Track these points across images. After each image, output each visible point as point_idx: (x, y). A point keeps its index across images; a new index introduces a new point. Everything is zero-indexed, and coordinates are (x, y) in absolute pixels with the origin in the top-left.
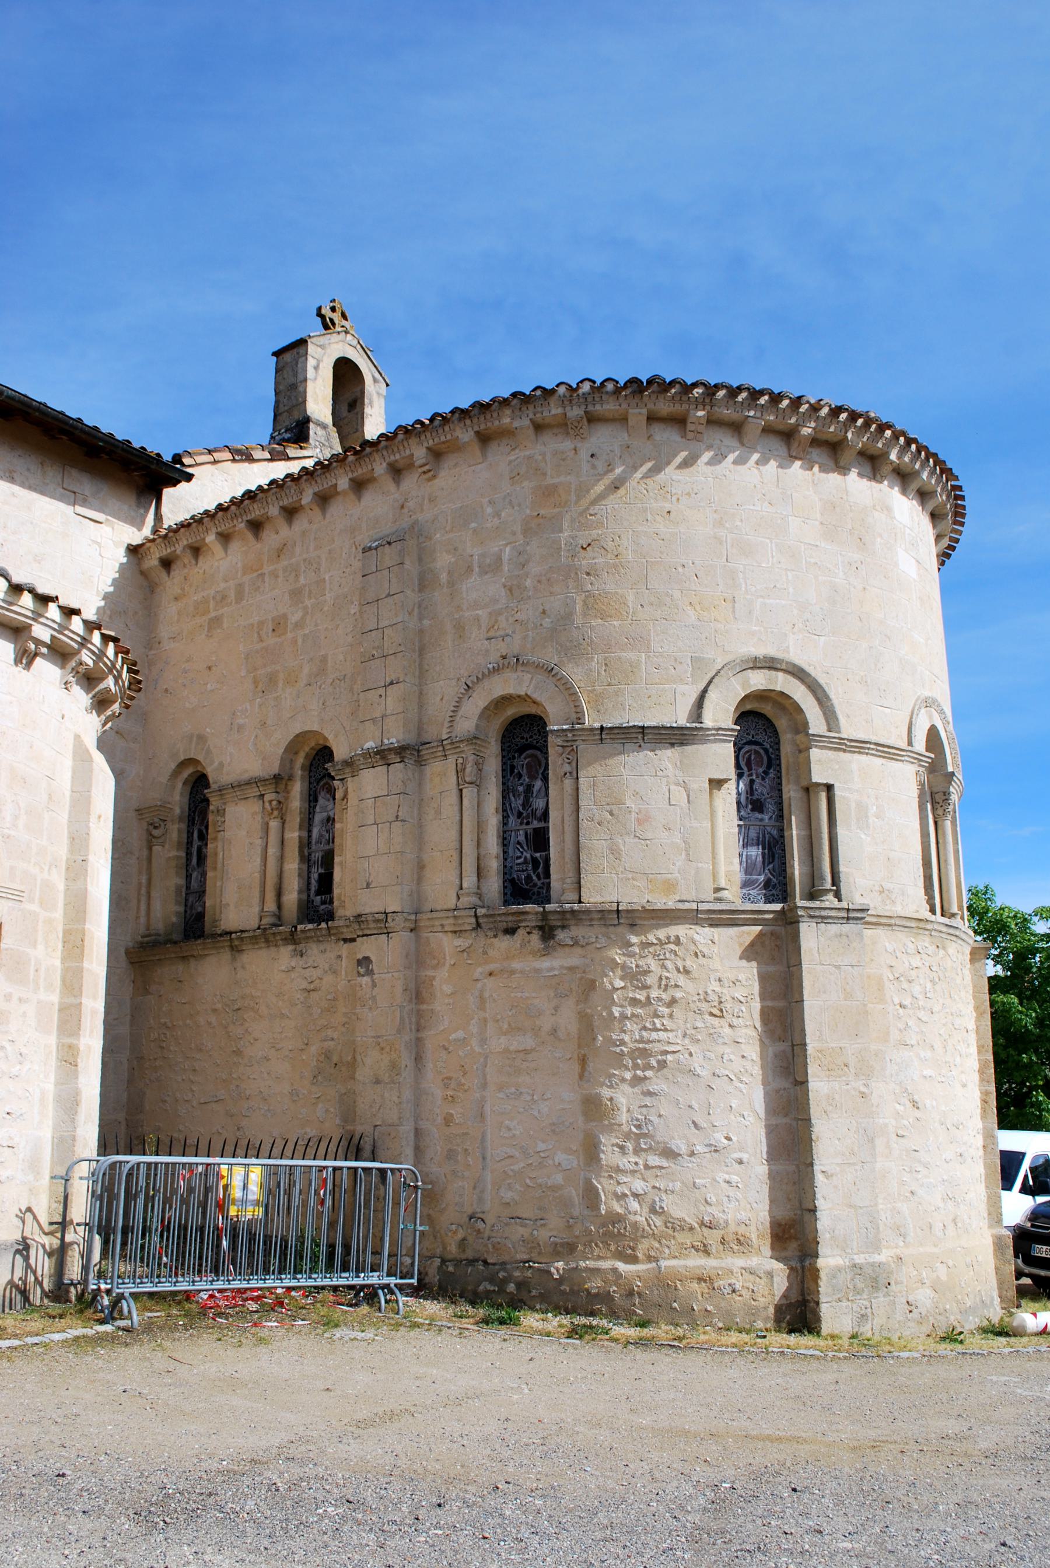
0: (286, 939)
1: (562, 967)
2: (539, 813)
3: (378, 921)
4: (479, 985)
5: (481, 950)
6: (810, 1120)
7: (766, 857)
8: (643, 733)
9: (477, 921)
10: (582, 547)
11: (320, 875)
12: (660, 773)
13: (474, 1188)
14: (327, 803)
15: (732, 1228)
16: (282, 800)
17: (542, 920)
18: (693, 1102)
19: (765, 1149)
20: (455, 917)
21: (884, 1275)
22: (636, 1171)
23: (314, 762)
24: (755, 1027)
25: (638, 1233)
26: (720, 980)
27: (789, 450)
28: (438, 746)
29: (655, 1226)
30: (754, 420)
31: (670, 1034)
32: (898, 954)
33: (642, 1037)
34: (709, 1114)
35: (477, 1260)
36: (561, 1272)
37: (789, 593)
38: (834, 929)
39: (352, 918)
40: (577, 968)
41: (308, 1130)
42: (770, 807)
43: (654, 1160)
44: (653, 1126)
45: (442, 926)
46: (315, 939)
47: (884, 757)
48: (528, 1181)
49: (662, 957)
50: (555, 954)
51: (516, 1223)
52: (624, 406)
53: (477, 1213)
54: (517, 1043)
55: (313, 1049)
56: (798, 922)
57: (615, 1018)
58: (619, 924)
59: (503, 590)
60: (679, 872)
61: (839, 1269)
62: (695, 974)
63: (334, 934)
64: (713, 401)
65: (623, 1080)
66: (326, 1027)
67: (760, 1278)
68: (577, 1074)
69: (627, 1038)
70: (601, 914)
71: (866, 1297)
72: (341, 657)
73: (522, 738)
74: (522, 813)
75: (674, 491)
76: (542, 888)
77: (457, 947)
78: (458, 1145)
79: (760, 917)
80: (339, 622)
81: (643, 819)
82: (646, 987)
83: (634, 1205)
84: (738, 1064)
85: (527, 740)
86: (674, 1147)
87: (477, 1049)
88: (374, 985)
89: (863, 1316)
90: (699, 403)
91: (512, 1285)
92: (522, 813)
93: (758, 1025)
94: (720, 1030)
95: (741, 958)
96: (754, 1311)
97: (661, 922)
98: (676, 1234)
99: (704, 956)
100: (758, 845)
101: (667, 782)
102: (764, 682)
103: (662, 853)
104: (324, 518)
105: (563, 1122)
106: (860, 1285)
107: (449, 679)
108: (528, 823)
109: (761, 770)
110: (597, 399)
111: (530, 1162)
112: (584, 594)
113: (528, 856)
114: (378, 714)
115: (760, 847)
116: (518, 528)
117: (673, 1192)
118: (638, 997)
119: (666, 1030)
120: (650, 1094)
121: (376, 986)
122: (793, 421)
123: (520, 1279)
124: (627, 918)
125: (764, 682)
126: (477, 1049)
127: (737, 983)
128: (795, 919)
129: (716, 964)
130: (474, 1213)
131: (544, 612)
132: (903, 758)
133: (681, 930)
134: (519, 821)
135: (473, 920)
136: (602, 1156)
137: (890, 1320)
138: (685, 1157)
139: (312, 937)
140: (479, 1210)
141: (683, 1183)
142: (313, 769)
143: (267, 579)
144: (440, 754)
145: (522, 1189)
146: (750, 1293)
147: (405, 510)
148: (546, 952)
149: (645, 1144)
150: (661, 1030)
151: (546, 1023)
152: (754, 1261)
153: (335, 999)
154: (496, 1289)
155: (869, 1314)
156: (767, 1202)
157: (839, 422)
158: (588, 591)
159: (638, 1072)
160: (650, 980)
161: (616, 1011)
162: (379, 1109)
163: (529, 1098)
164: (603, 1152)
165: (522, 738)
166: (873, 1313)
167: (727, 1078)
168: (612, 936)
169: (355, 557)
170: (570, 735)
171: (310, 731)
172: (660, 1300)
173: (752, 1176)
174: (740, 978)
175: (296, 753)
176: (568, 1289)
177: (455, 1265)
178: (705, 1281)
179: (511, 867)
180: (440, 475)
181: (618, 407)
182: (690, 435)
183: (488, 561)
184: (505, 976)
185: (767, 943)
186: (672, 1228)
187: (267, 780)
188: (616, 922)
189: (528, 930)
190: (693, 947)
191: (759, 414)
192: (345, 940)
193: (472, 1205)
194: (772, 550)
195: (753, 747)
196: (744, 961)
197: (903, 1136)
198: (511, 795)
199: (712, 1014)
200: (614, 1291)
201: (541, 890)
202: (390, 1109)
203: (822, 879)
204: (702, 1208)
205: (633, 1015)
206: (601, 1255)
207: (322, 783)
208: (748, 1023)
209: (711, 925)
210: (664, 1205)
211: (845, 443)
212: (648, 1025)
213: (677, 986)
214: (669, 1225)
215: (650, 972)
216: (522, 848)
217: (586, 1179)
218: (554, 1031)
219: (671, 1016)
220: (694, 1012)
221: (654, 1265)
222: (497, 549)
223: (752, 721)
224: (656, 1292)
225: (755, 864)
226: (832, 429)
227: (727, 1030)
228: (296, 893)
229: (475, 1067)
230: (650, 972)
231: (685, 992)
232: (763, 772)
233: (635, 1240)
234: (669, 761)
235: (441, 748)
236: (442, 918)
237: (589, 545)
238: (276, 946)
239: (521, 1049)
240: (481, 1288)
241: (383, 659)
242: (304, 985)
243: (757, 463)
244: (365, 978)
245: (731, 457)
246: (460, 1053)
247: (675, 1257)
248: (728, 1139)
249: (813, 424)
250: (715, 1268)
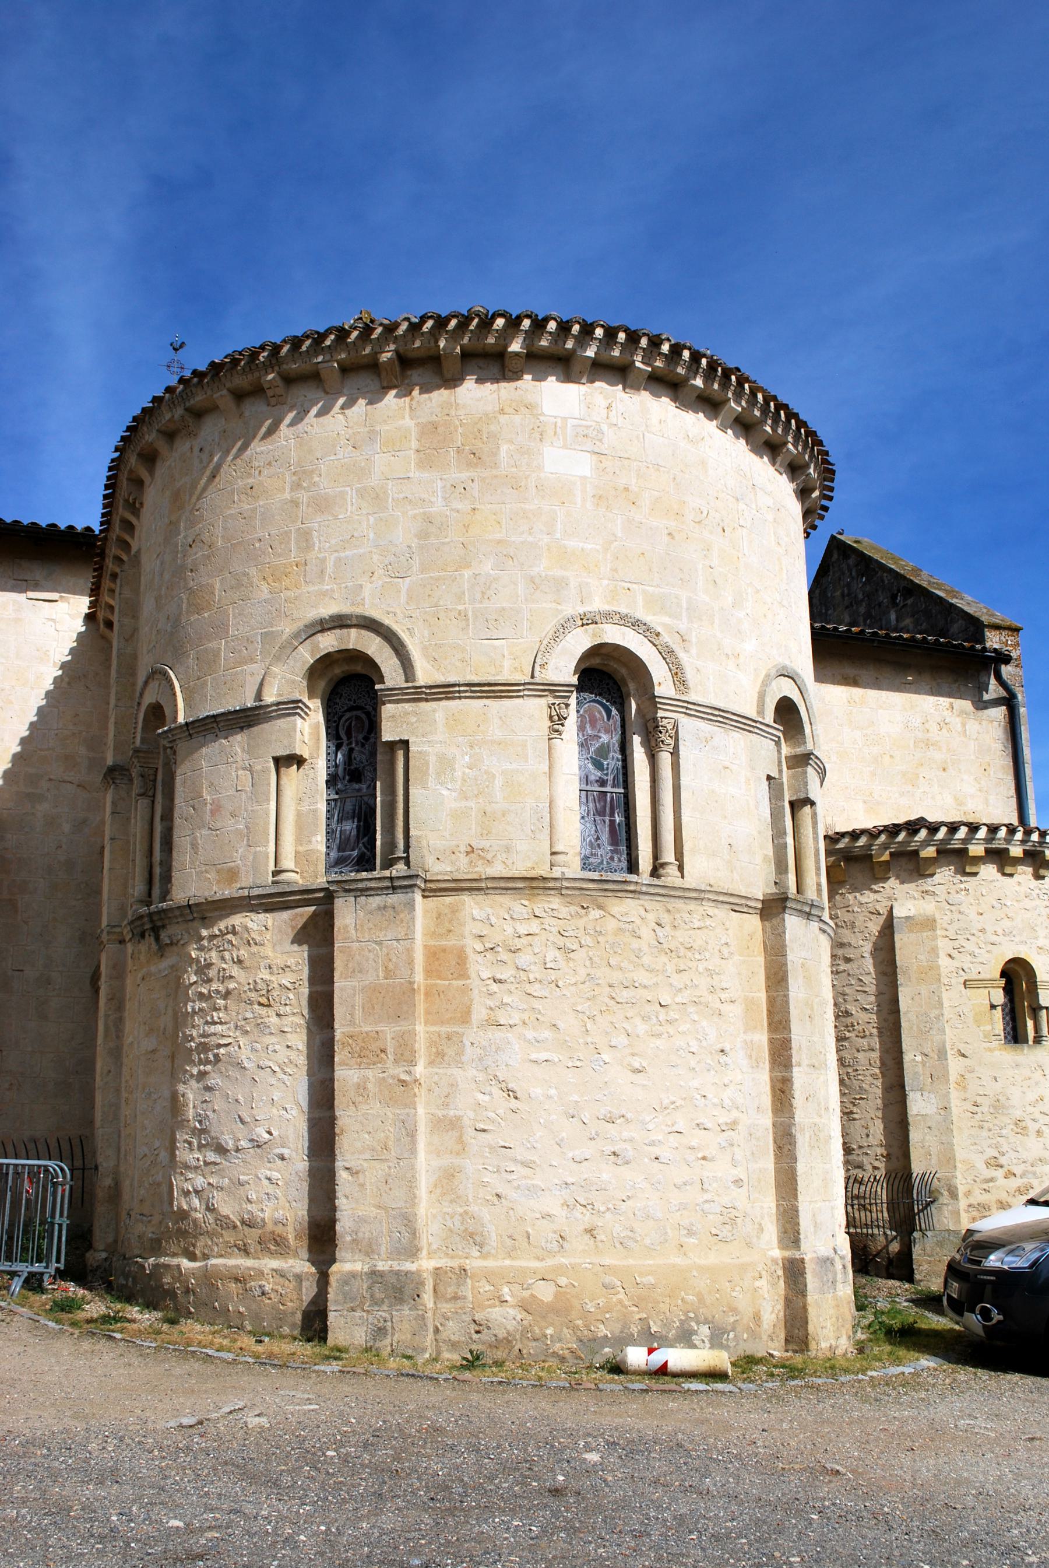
7: (362, 829)
8: (215, 721)
15: (270, 1227)
18: (240, 1097)
19: (306, 1145)
21: (411, 1286)
24: (303, 1015)
25: (198, 1231)
26: (270, 968)
30: (325, 365)
31: (225, 1027)
32: (493, 920)
37: (369, 539)
38: (376, 901)
43: (212, 1157)
44: (209, 1121)
47: (487, 697)
49: (221, 949)
52: (209, 393)
58: (194, 919)
60: (241, 860)
61: (353, 1275)
62: (247, 964)
65: (192, 1076)
71: (386, 1308)
83: (196, 1202)
84: (283, 1054)
86: (223, 1143)
89: (380, 1329)
90: (269, 366)
93: (305, 1012)
94: (266, 1020)
95: (292, 943)
97: (224, 913)
98: (223, 1232)
99: (256, 944)
100: (353, 818)
102: (335, 643)
103: (227, 842)
106: (379, 1295)
109: (360, 737)
110: (189, 394)
115: (356, 820)
117: (222, 1188)
119: (221, 1023)
120: (208, 1089)
122: (368, 350)
124: (197, 912)
125: (335, 643)
129: (268, 951)
132: (521, 694)
133: (237, 920)
137: (417, 1337)
138: (233, 1153)
146: (279, 1297)
155: (389, 1329)
156: (306, 1201)
157: (423, 334)
166: (393, 1328)
174: (289, 964)
178: (240, 1281)
181: (205, 396)
182: (273, 401)
190: (246, 936)
191: (328, 357)
194: (352, 498)
195: (355, 713)
196: (296, 945)
197: (484, 1131)
199: (260, 1004)
204: (244, 1206)
208: (295, 1011)
209: (266, 911)
210: (215, 1202)
213: (231, 977)
214: (218, 1222)
223: (355, 685)
225: (349, 839)
226: (417, 344)
227: (274, 1019)
231: (237, 982)
232: (363, 739)
233: (195, 1237)
234: (239, 746)
243: (342, 408)
245: (314, 411)
247: (221, 1256)
249: (392, 347)
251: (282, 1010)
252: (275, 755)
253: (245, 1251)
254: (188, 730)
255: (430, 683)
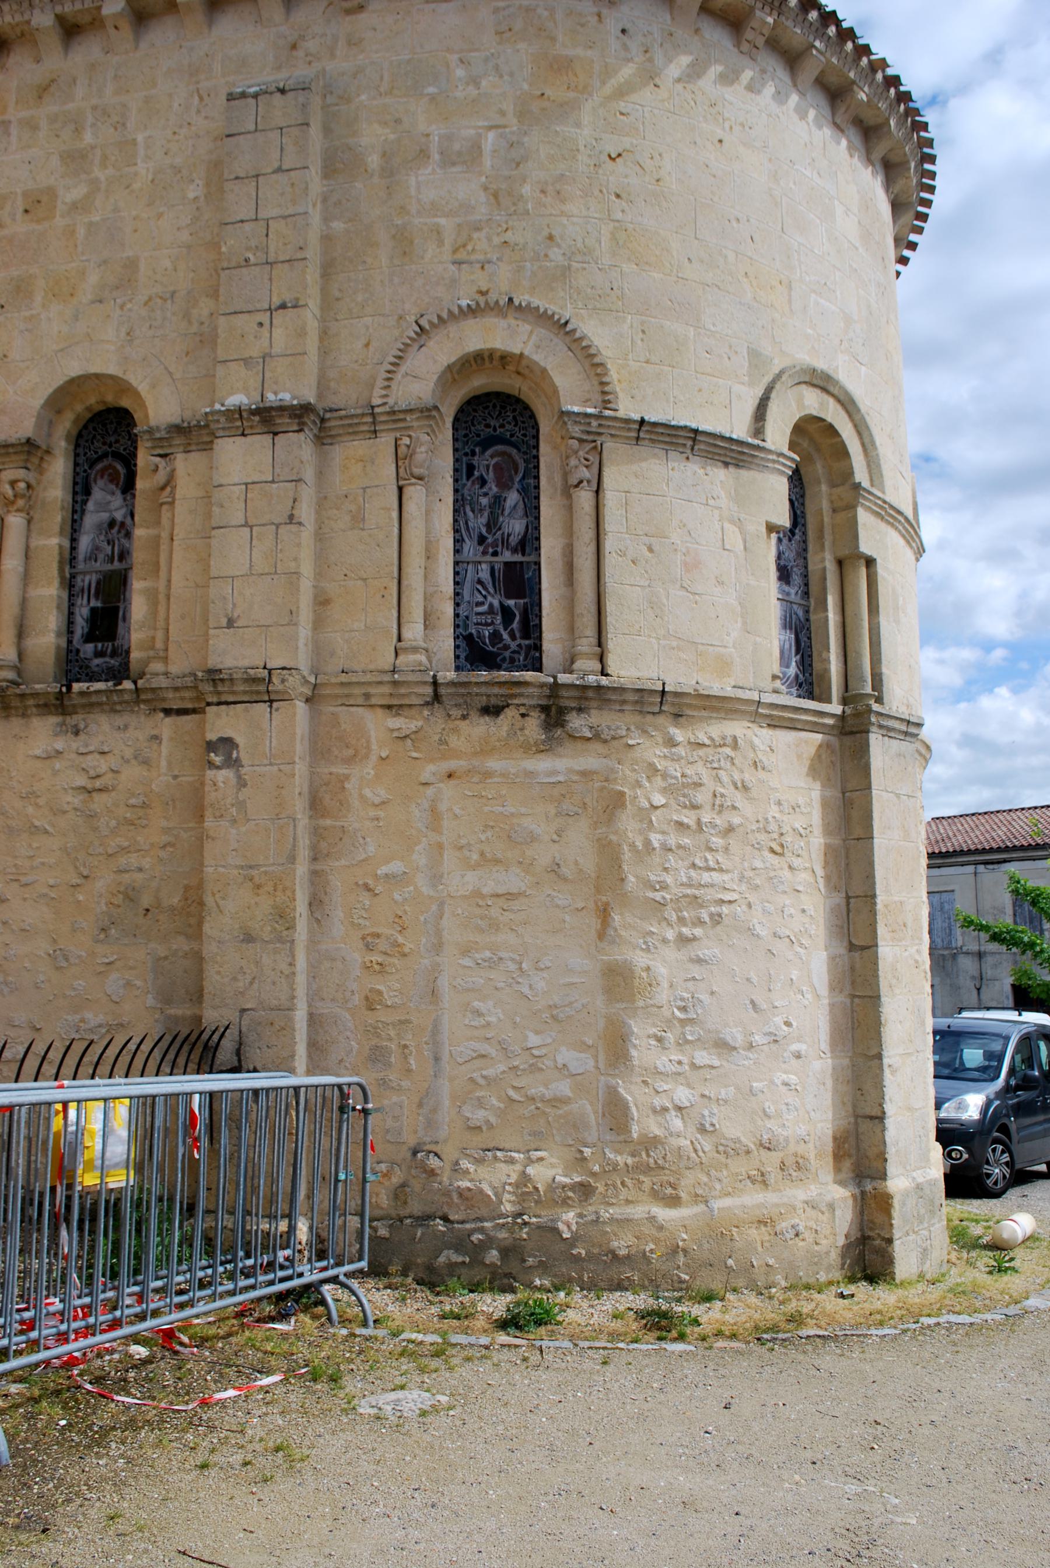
0: (46, 705)
1: (570, 771)
2: (514, 540)
3: (255, 680)
4: (430, 791)
5: (436, 738)
6: (879, 997)
8: (694, 440)
9: (436, 692)
10: (610, 156)
11: (93, 610)
12: (711, 502)
13: (420, 1105)
14: (109, 497)
15: (792, 1148)
16: (33, 482)
17: (549, 697)
20: (395, 683)
22: (679, 1074)
23: (84, 433)
27: (833, 114)
28: (363, 415)
29: (704, 1152)
31: (726, 877)
33: (690, 878)
34: (770, 990)
35: (430, 1217)
36: (574, 1228)
39: (200, 674)
40: (595, 773)
41: (89, 1015)
42: (796, 579)
43: (702, 1057)
44: (703, 1008)
45: (367, 696)
46: (107, 708)
48: (511, 1093)
49: (716, 765)
50: (560, 749)
51: (495, 1157)
53: (425, 1143)
54: (494, 881)
55: (101, 884)
56: (868, 732)
57: (654, 849)
58: (661, 712)
59: (482, 194)
60: (734, 647)
62: (754, 793)
63: (145, 701)
64: (783, 7)
65: (665, 941)
66: (125, 850)
67: (823, 1213)
68: (593, 931)
69: (669, 880)
70: (638, 694)
72: (167, 263)
73: (488, 426)
74: (487, 538)
75: (726, 115)
76: (519, 653)
77: (393, 730)
78: (390, 1039)
79: (821, 721)
80: (161, 210)
81: (692, 565)
82: (695, 807)
83: (677, 1123)
85: (495, 430)
87: (425, 890)
88: (242, 783)
91: (495, 1252)
92: (487, 538)
96: (816, 1259)
97: (715, 715)
98: (729, 1161)
99: (763, 769)
101: (720, 515)
104: (137, 48)
105: (571, 1003)
107: (383, 315)
108: (495, 554)
111: (516, 1063)
112: (612, 224)
113: (496, 603)
114: (255, 352)
116: (509, 107)
117: (726, 1101)
118: (686, 820)
119: (721, 870)
120: (699, 961)
121: (245, 785)
123: (507, 1243)
124: (673, 704)
125: (816, 406)
126: (425, 890)
127: (797, 809)
128: (862, 728)
130: (419, 1144)
131: (551, 238)
133: (737, 728)
134: (481, 549)
135: (429, 690)
136: (634, 1053)
139: (100, 704)
140: (428, 1139)
141: (738, 1088)
142: (82, 442)
143: (14, 130)
144: (365, 428)
145: (502, 1105)
147: (300, 53)
148: (545, 748)
149: (692, 1034)
150: (714, 869)
151: (543, 855)
152: (812, 1191)
153: (144, 806)
154: (467, 1260)
158: (618, 221)
159: (684, 930)
160: (701, 797)
161: (655, 839)
162: (251, 983)
163: (512, 967)
164: (635, 1046)
165: (488, 426)
167: (787, 940)
168: (650, 729)
169: (199, 111)
170: (594, 423)
171: (97, 376)
172: (711, 1257)
173: (811, 1074)
175: (59, 412)
176: (583, 1252)
177: (391, 1226)
178: (765, 1224)
179: (467, 617)
180: (370, 8)
183: (457, 147)
184: (475, 780)
185: (824, 757)
186: (725, 1152)
187: (13, 445)
188: (656, 709)
189: (523, 710)
192: (168, 712)
193: (416, 1132)
198: (468, 508)
200: (652, 1251)
201: (516, 656)
202: (274, 983)
203: (862, 679)
205: (680, 847)
206: (630, 1198)
207: (100, 466)
211: (885, 130)
212: (698, 862)
213: (734, 808)
214: (721, 1148)
215: (701, 785)
216: (485, 589)
217: (608, 1087)
218: (555, 870)
219: (727, 849)
220: (753, 845)
221: (701, 1208)
222: (472, 132)
224: (706, 1246)
227: (786, 874)
228: (53, 635)
229: (422, 919)
230: (701, 785)
231: (743, 816)
235: (369, 419)
236: (369, 683)
237: (619, 155)
238: (24, 715)
239: (500, 892)
240: (442, 1259)
241: (268, 267)
242: (81, 781)
244: (224, 772)
246: (397, 897)
248: (788, 1024)
250: (777, 1205)
251: (796, 862)
252: (769, 520)
253: (761, 1180)
254: (639, 430)
255: (895, 505)
